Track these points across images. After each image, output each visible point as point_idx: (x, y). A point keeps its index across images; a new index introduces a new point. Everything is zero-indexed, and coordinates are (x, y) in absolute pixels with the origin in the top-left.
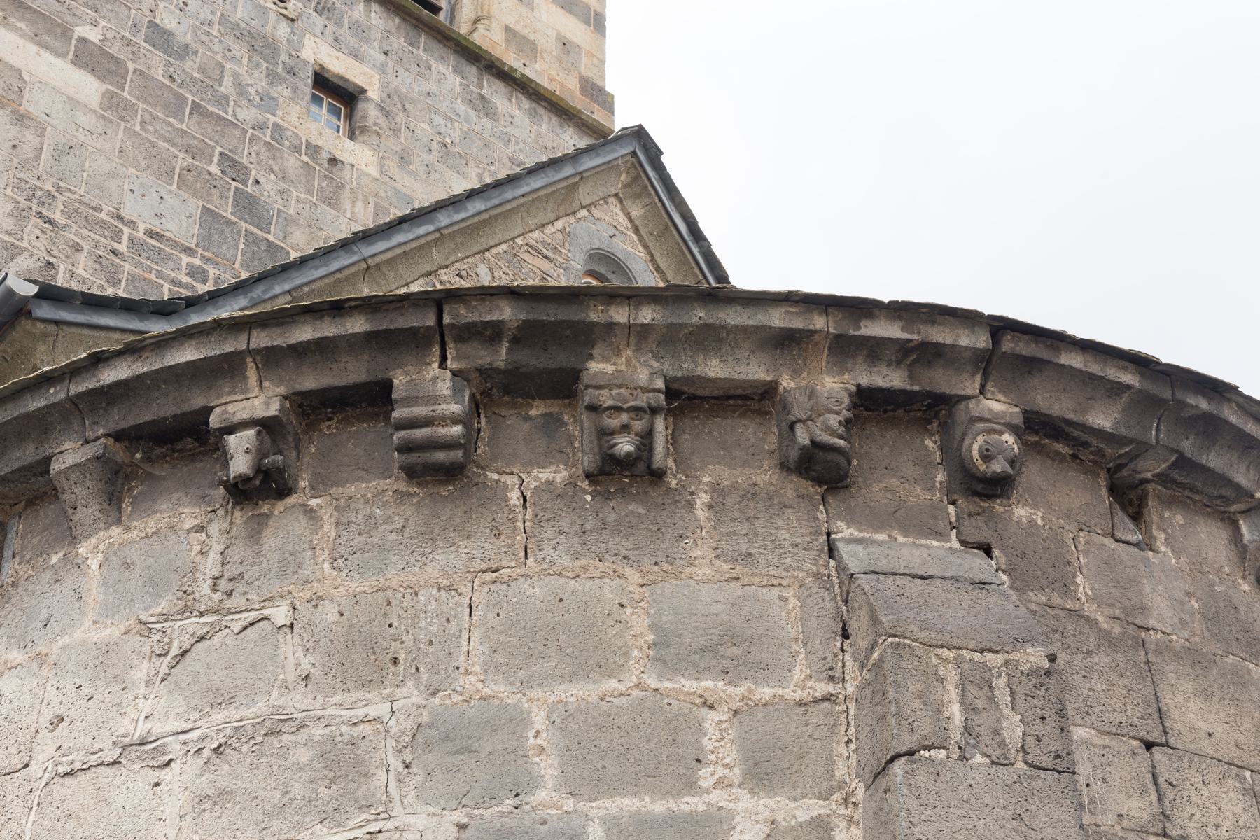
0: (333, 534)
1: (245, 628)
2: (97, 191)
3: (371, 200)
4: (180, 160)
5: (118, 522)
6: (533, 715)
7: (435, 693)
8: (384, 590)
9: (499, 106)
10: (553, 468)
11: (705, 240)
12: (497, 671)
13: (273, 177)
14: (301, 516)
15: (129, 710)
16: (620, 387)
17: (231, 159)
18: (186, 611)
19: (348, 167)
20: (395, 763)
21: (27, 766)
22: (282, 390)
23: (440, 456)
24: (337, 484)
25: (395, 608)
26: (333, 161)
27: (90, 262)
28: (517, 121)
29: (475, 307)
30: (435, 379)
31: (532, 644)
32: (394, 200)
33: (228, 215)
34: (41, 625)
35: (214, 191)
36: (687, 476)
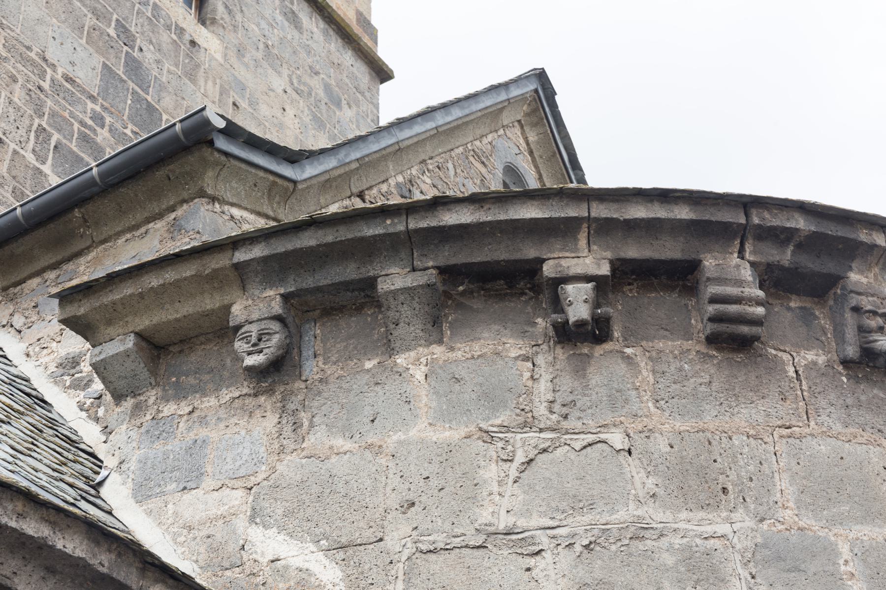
0: (652, 381)
1: (585, 447)
2: (29, 33)
3: (218, 81)
4: (88, 19)
5: (440, 342)
6: (840, 546)
7: (762, 520)
8: (703, 432)
9: (304, 22)
11: (581, 170)
12: (807, 509)
13: (151, 47)
14: (620, 361)
15: (485, 503)
16: (873, 296)
17: (123, 26)
18: (525, 425)
19: (203, 50)
20: (744, 574)
21: (381, 540)
22: (609, 255)
24: (647, 339)
25: (716, 448)
26: (193, 43)
27: (23, 94)
28: (315, 36)
29: (776, 214)
30: (738, 266)
31: (829, 491)
32: (233, 84)
33: (120, 73)
34: (367, 420)
35: (111, 51)
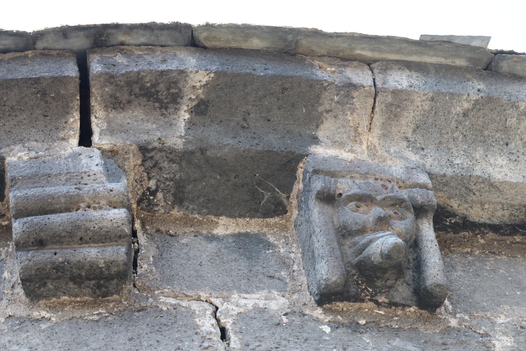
10: (264, 293)
23: (92, 253)
36: (471, 315)
